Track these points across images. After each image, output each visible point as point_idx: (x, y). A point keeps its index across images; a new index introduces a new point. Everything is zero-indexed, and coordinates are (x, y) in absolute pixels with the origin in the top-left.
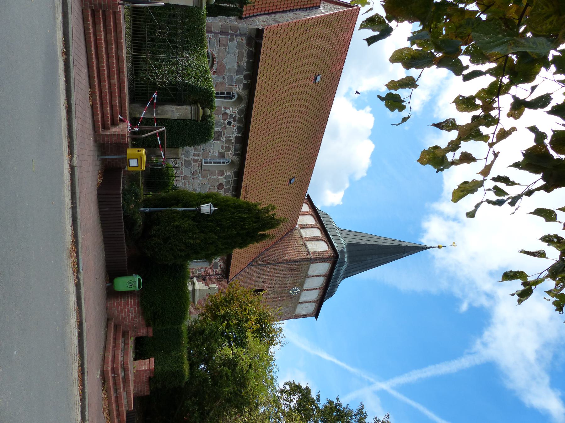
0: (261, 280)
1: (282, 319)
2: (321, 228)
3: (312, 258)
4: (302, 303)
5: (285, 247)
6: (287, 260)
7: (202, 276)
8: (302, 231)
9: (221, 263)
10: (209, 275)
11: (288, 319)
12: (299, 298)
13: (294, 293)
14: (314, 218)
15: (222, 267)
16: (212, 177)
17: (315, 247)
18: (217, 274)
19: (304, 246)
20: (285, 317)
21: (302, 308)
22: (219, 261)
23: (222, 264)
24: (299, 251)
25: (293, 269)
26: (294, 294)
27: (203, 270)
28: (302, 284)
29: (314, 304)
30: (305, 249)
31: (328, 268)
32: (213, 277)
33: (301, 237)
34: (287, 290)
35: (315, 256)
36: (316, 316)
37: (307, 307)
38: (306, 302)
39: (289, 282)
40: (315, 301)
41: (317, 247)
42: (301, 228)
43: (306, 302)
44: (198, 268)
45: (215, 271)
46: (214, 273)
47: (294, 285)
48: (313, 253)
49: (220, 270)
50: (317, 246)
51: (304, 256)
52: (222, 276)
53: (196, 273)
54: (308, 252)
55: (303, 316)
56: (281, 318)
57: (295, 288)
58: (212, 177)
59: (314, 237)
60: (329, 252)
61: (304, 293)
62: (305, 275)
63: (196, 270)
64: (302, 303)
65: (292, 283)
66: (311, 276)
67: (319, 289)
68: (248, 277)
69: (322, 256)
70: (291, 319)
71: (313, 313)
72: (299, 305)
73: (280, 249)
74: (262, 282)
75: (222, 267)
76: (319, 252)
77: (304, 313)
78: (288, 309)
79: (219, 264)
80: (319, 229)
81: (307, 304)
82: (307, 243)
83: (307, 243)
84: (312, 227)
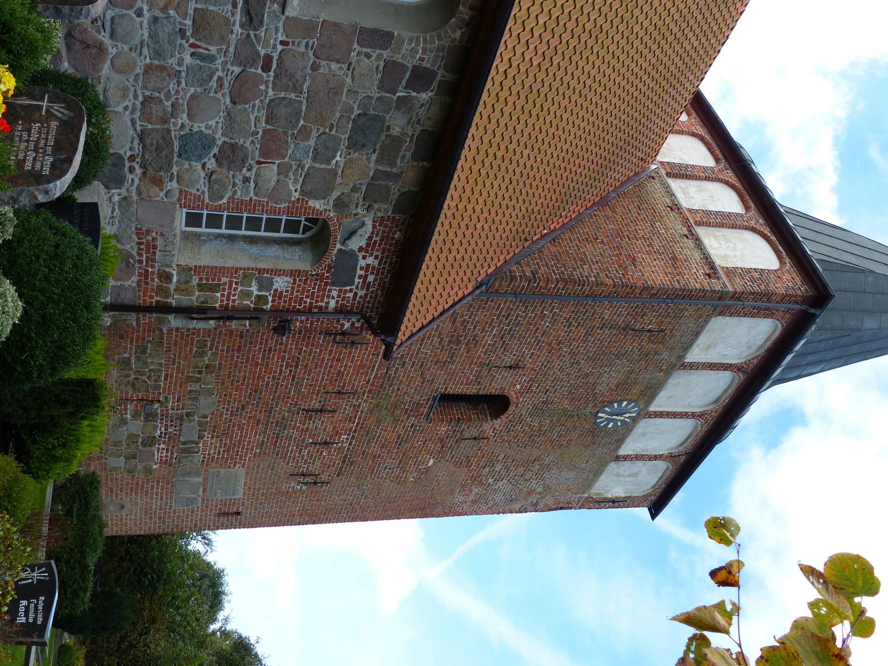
0: (508, 360)
1: (541, 505)
2: (738, 185)
3: (727, 293)
4: (626, 458)
5: (619, 234)
6: (633, 288)
7: (275, 310)
8: (675, 185)
9: (370, 260)
10: (308, 311)
11: (561, 508)
12: (621, 441)
13: (615, 421)
14: (710, 149)
15: (371, 278)
16: (274, 66)
17: (729, 253)
18: (341, 311)
19: (690, 243)
20: (551, 502)
21: (618, 475)
22: (361, 249)
23: (376, 262)
24: (674, 259)
25: (642, 330)
26: (610, 425)
27: (281, 283)
28: (651, 392)
29: (662, 466)
30: (697, 255)
31: (760, 342)
32: (324, 322)
33: (675, 207)
34: (589, 409)
35: (738, 285)
36: (656, 509)
37: (635, 475)
38: (638, 457)
39: (609, 378)
40: (671, 457)
41: (738, 253)
42: (669, 175)
43: (638, 457)
44: (260, 271)
45: (335, 293)
46: (332, 304)
47: (621, 390)
48: (731, 272)
49: (361, 293)
50: (734, 249)
51: (696, 279)
52: (367, 320)
53: (248, 294)
54: (712, 265)
55: (613, 502)
56: (536, 504)
57: (619, 405)
58: (274, 66)
59: (722, 214)
60: (786, 277)
61: (644, 425)
62: (673, 360)
63: (246, 278)
64: (626, 458)
65: (617, 385)
66: (693, 366)
67: (701, 415)
68: (459, 342)
69: (763, 287)
70: (571, 508)
71: (650, 495)
72: (613, 466)
73: (602, 242)
74: (510, 367)
75: (371, 278)
76: (749, 271)
77: (618, 492)
78: (572, 474)
79: (362, 263)
80: (732, 187)
81: (639, 464)
82: (701, 231)
83: (701, 231)
84: (707, 179)
